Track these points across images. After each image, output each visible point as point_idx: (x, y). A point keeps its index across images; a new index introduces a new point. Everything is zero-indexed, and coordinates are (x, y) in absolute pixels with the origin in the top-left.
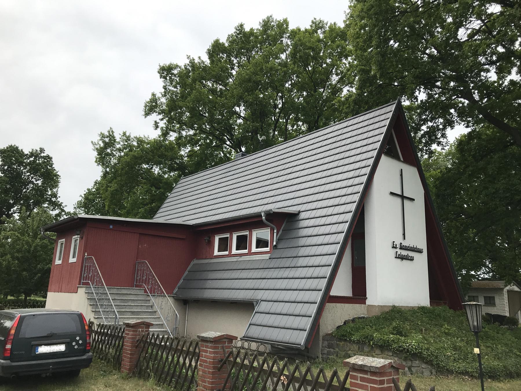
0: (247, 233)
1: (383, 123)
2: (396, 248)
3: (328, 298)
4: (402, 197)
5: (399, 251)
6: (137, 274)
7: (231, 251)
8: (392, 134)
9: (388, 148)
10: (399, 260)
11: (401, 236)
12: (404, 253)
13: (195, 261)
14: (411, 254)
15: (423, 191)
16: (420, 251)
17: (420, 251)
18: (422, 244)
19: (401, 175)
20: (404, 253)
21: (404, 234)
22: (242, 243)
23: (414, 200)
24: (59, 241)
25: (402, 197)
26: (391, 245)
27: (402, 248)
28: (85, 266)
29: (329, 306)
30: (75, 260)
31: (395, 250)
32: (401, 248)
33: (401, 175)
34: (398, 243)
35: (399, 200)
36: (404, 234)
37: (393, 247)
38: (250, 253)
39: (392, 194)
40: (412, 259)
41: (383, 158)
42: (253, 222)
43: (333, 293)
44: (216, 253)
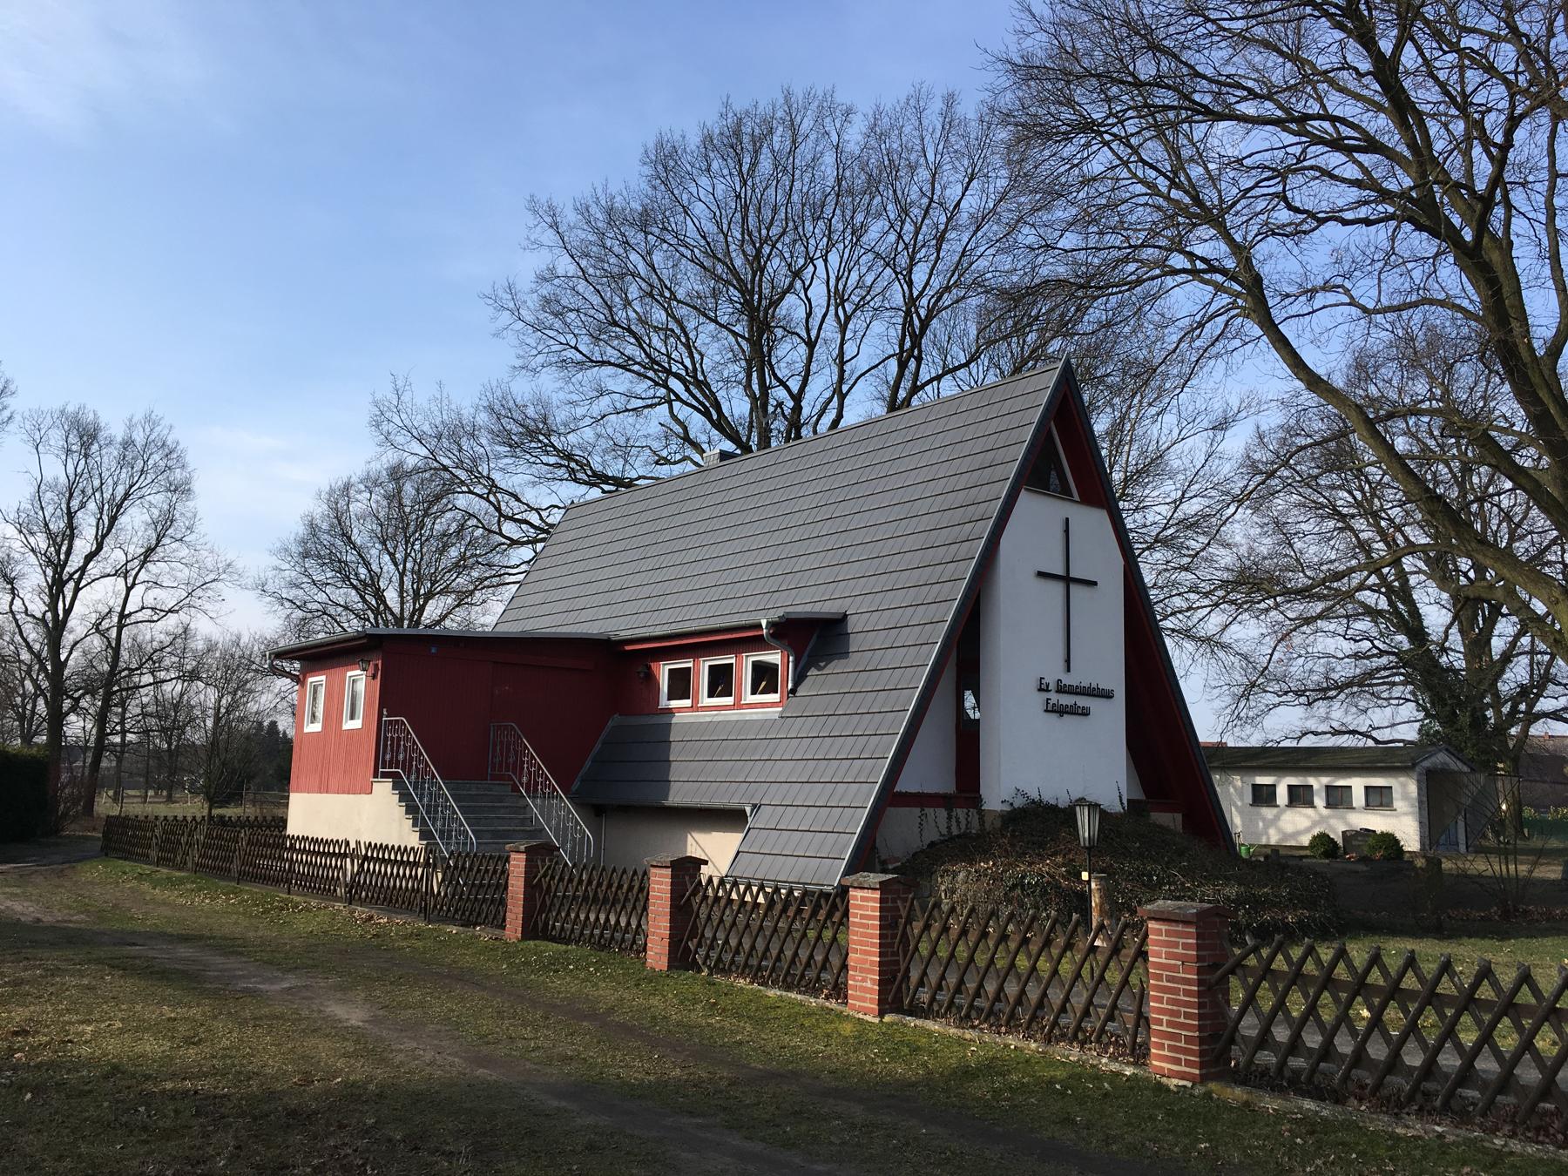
0: (730, 659)
1: (1014, 436)
2: (1048, 690)
3: (889, 797)
4: (1067, 580)
5: (1055, 697)
6: (494, 750)
7: (696, 700)
8: (1050, 431)
9: (1038, 472)
10: (1054, 716)
11: (1061, 664)
12: (1066, 700)
13: (616, 720)
14: (1082, 701)
15: (1122, 562)
16: (1108, 695)
17: (1108, 695)
18: (1114, 678)
19: (1067, 531)
20: (1066, 700)
21: (1068, 661)
22: (721, 681)
23: (1095, 583)
24: (310, 680)
25: (1067, 580)
26: (1034, 684)
27: (1062, 689)
28: (386, 738)
29: (892, 812)
30: (357, 724)
31: (1045, 695)
32: (1058, 691)
33: (1067, 531)
34: (1051, 680)
35: (1057, 588)
36: (1068, 661)
37: (1040, 690)
38: (738, 705)
39: (1041, 574)
40: (1085, 713)
41: (1025, 498)
42: (743, 639)
43: (905, 785)
44: (664, 702)
